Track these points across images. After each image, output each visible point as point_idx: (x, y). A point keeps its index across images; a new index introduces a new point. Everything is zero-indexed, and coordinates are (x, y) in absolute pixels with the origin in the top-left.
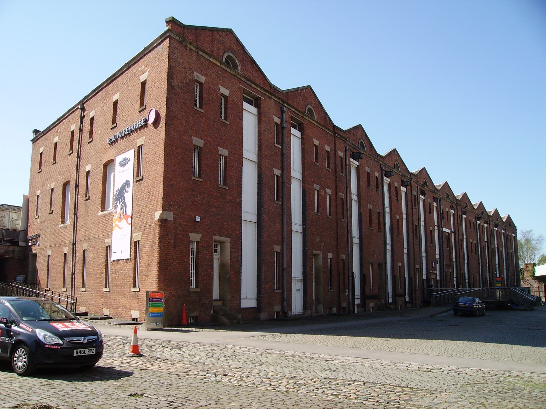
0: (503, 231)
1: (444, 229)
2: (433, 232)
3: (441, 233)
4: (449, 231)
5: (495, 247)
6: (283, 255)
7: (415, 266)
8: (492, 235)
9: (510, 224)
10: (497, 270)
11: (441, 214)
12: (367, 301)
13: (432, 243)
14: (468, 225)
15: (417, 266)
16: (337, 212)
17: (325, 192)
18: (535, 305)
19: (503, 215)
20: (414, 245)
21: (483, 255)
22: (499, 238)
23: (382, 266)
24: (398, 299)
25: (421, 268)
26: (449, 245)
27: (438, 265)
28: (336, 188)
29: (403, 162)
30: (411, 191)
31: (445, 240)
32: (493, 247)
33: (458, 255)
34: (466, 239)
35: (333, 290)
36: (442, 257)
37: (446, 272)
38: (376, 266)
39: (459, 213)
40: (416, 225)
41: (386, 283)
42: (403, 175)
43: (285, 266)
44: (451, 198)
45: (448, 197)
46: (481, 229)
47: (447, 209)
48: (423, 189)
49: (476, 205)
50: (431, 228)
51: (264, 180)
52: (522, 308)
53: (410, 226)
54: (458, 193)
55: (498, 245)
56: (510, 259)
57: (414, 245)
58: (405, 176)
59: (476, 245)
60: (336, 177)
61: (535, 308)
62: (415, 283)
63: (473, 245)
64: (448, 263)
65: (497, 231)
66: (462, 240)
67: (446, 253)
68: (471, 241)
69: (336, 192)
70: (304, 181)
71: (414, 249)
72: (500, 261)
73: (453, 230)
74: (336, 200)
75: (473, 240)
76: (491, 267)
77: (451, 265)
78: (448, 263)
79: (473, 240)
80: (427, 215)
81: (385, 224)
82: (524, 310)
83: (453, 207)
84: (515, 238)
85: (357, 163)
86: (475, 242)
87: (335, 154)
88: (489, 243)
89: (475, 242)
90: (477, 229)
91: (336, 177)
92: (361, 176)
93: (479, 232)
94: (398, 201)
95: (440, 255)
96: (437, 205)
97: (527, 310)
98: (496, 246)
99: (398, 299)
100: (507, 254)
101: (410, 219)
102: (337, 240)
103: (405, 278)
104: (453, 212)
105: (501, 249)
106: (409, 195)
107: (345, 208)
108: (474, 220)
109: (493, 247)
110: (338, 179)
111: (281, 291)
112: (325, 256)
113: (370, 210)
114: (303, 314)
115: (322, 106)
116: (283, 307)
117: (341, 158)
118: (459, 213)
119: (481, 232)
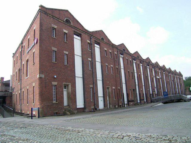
1: (157, 77)
4: (159, 78)
8: (174, 78)
9: (180, 75)
11: (155, 72)
12: (129, 103)
15: (148, 90)
23: (134, 90)
24: (141, 101)
27: (156, 89)
38: (132, 90)
39: (162, 72)
42: (140, 60)
44: (159, 67)
50: (152, 77)
53: (145, 76)
58: (141, 60)
62: (148, 94)
63: (168, 82)
65: (160, 72)
66: (164, 80)
69: (115, 65)
77: (160, 89)
84: (182, 79)
99: (141, 101)
100: (180, 84)
101: (144, 74)
112: (112, 88)
114: (104, 108)
116: (95, 106)
117: (116, 54)
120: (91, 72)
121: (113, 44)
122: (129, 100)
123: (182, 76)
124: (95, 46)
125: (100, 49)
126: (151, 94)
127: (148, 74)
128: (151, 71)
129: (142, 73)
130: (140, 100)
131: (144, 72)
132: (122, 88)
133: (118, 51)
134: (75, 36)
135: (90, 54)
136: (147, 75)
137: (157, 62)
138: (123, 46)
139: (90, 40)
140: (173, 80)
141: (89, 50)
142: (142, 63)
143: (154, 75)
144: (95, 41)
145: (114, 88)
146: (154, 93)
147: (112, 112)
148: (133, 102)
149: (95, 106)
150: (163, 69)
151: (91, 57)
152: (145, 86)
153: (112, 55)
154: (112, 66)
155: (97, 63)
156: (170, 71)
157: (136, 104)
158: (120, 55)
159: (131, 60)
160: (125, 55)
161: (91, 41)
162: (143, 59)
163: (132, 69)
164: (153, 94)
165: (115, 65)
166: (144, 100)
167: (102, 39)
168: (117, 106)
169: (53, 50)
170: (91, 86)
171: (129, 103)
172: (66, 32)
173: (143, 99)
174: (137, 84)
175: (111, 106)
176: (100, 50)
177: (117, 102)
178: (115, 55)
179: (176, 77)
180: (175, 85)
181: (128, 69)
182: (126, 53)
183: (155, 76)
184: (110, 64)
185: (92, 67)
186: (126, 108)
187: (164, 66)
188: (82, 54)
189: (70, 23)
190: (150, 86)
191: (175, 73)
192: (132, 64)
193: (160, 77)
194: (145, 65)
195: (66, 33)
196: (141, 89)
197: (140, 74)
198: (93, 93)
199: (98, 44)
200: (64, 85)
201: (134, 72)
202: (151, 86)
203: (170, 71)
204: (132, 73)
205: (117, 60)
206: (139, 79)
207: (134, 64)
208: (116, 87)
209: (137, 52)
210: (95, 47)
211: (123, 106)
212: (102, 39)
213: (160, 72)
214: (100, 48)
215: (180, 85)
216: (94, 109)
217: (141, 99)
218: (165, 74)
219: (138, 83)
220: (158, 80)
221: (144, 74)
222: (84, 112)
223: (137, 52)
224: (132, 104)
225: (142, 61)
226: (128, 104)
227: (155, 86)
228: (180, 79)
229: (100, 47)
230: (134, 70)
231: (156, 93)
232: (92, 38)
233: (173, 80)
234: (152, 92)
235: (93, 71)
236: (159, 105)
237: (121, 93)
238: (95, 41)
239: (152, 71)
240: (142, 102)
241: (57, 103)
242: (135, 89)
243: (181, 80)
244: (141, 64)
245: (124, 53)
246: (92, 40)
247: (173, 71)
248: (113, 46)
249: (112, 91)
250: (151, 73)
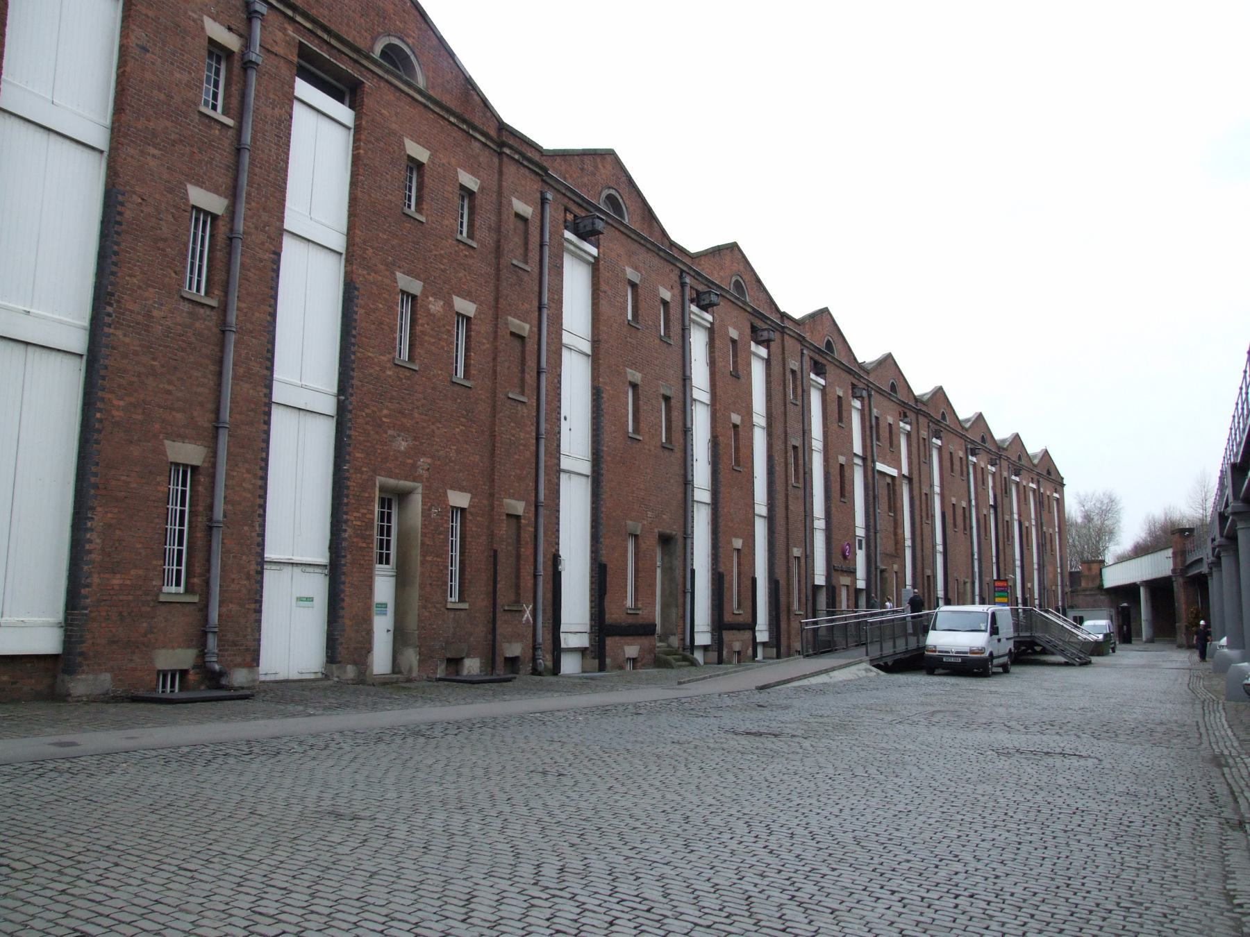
0: (1034, 486)
1: (880, 466)
2: (846, 468)
3: (870, 473)
4: (894, 472)
5: (1012, 518)
6: (213, 477)
7: (788, 551)
8: (1007, 491)
9: (1046, 473)
10: (1018, 571)
11: (871, 428)
12: (609, 641)
13: (842, 494)
14: (947, 464)
15: (797, 552)
16: (495, 372)
17: (449, 304)
18: (1100, 654)
19: (1033, 448)
20: (787, 496)
21: (982, 531)
22: (1023, 500)
23: (674, 543)
24: (727, 636)
25: (809, 556)
26: (894, 506)
27: (860, 556)
28: (497, 300)
29: (759, 281)
30: (784, 359)
31: (882, 493)
32: (1007, 518)
33: (918, 533)
34: (942, 495)
35: (465, 606)
36: (872, 534)
37: (882, 571)
38: (651, 542)
39: (924, 434)
40: (795, 448)
41: (689, 592)
42: (756, 313)
43: (219, 514)
44: (901, 395)
45: (1049, 473)
46: (979, 476)
47: (890, 420)
48: (821, 360)
49: (1035, 456)
50: (842, 459)
51: (128, 214)
52: (1062, 659)
53: (779, 446)
54: (1001, 432)
55: (1020, 515)
56: (1048, 547)
57: (787, 496)
58: (764, 318)
59: (966, 513)
60: (498, 270)
61: (1094, 659)
62: (789, 594)
63: (959, 512)
64: (890, 548)
65: (994, 474)
66: (928, 498)
67: (883, 523)
68: (954, 500)
69: (496, 311)
70: (356, 256)
71: (787, 508)
72: (1025, 551)
73: (905, 471)
74: (496, 338)
75: (959, 500)
76: (1002, 565)
77: (898, 554)
78: (890, 548)
79: (959, 500)
80: (980, 489)
81: (971, 528)
82: (1066, 664)
83: (905, 416)
84: (1060, 502)
85: (594, 251)
86: (964, 504)
87: (500, 205)
88: (999, 510)
89: (964, 504)
90: (968, 474)
91: (498, 270)
92: (604, 287)
93: (975, 483)
94: (736, 375)
95: (867, 528)
96: (863, 405)
97: (1073, 665)
98: (1016, 516)
99: (727, 636)
100: (1042, 536)
101: (779, 430)
102: (493, 453)
103: (754, 581)
104: (908, 427)
105: (1027, 524)
106: (777, 369)
107: (531, 363)
108: (961, 454)
109: (1007, 518)
110: (504, 273)
111: (196, 599)
112: (435, 497)
113: (842, 466)
114: (326, 676)
115: (451, 55)
116: (202, 654)
117: (524, 220)
118: (924, 434)
119: (980, 483)
120: (207, 323)
121: (502, 127)
122: (613, 615)
123: (1059, 484)
124: (291, 98)
125: (356, 140)
126: (816, 588)
127: (806, 432)
128: (836, 415)
129: (759, 419)
130: (719, 625)
131: (778, 411)
132: (546, 509)
133: (544, 201)
134: (303, 89)
135: (222, 156)
136: (798, 443)
137: (889, 358)
138: (606, 171)
139: (239, 25)
140: (995, 507)
141: (218, 115)
142: (766, 343)
143: (857, 448)
144: (303, 51)
145: (459, 499)
146: (845, 580)
147: (681, 693)
148: (646, 641)
149: (202, 654)
150: (933, 413)
151: (224, 181)
152: (770, 519)
153: (486, 217)
154: (465, 306)
155: (292, 257)
156: (978, 440)
157: (673, 655)
158: (568, 235)
159: (666, 295)
160: (614, 244)
161: (246, 38)
162: (784, 316)
163: (674, 373)
164: (832, 590)
165: (497, 307)
166: (752, 626)
167: (391, 53)
168: (472, 666)
169: (199, 210)
170: (190, 453)
171: (609, 641)
172: (422, 155)
173: (745, 618)
174: (702, 493)
175: (411, 657)
176: (356, 148)
177: (480, 630)
178: (510, 224)
179: (1017, 484)
180: (1009, 537)
181: (634, 365)
182: (630, 234)
183: (864, 459)
184: (443, 288)
185: (219, 277)
186: (579, 684)
187: (939, 393)
188: (118, 130)
189: (409, 69)
190: (820, 524)
191: (1011, 456)
192: (676, 328)
193: (899, 468)
194: (794, 364)
195: (419, 166)
196: (738, 543)
197: (736, 419)
198: (201, 520)
199: (342, 88)
200: (382, 489)
201: (686, 402)
202: (828, 531)
203: (978, 440)
204: (667, 399)
205: (532, 267)
206: (728, 461)
207: (698, 342)
208: (488, 487)
209: (825, 311)
210: (297, 107)
211: (545, 661)
212: (391, 53)
213: (908, 435)
214: (358, 129)
215: (1041, 547)
216: (192, 677)
217: (728, 618)
218: (946, 456)
219: (715, 492)
220: (882, 492)
221: (779, 430)
222: (56, 696)
223: (825, 311)
224: (632, 650)
225: (767, 323)
226: (597, 653)
227: (860, 532)
228: (1041, 502)
229: (358, 118)
230: (686, 379)
231: (861, 584)
232: (549, 196)
233: (995, 507)
234: (830, 569)
235: (224, 309)
236: (840, 676)
237: (527, 551)
238: (303, 51)
239: (740, 376)
240: (736, 641)
241: (465, 606)
242: (675, 531)
243: (1050, 511)
244: (763, 352)
245: (600, 225)
246: (257, 25)
247: (1003, 441)
248: (507, 144)
249: (434, 528)
250: (834, 426)
